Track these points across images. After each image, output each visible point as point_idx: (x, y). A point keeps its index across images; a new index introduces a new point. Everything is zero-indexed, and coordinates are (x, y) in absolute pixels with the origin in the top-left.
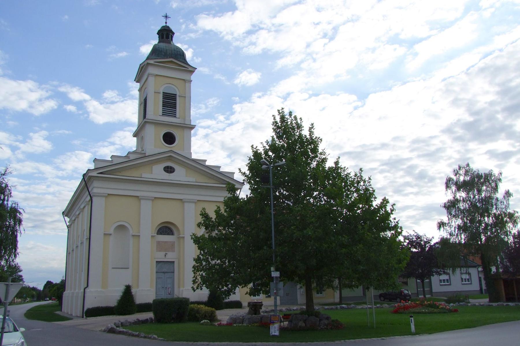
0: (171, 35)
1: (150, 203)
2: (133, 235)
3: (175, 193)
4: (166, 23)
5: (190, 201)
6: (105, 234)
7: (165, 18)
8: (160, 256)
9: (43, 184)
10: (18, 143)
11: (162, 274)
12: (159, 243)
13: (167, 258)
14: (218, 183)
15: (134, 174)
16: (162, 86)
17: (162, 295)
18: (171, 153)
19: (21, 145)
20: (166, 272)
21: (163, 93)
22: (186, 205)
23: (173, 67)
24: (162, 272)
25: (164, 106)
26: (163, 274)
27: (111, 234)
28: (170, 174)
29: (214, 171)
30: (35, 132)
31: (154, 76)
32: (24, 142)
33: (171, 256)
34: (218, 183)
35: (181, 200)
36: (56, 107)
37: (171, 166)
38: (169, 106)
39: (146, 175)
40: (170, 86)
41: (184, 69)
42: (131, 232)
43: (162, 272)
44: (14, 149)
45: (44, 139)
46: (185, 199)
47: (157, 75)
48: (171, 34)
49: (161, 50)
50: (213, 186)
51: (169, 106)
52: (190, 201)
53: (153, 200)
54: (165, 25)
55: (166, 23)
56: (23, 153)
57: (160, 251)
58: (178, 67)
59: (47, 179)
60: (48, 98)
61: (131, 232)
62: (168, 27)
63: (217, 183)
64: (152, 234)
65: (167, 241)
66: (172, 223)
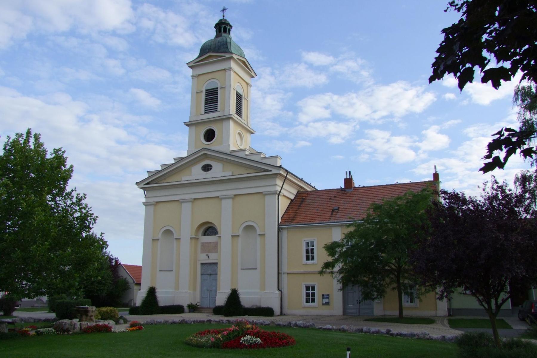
0: (229, 29)
1: (189, 205)
2: (259, 235)
3: (182, 194)
4: (224, 16)
5: (227, 198)
6: (153, 240)
7: (225, 11)
8: (203, 258)
9: (456, 179)
10: (417, 143)
11: (207, 275)
12: (203, 244)
13: (210, 259)
14: (257, 171)
15: (175, 179)
16: (204, 84)
17: (207, 297)
18: (204, 150)
19: (420, 145)
20: (211, 274)
21: (206, 90)
22: (223, 201)
23: (212, 61)
24: (208, 274)
25: (206, 103)
26: (208, 276)
27: (158, 240)
28: (208, 172)
29: (247, 160)
30: (426, 129)
31: (196, 77)
32: (421, 141)
33: (213, 258)
34: (257, 171)
35: (218, 197)
36: (435, 99)
37: (208, 163)
38: (211, 102)
39: (185, 178)
40: (216, 81)
41: (224, 58)
42: (258, 232)
43: (208, 274)
44: (416, 149)
45: (438, 133)
46: (264, 192)
47: (199, 75)
48: (229, 27)
49: (206, 48)
50: (253, 176)
51: (211, 102)
52: (227, 198)
53: (233, 198)
54: (222, 18)
55: (224, 16)
56: (424, 152)
57: (203, 253)
58: (215, 60)
59: (456, 174)
60: (424, 93)
61: (258, 232)
62: (226, 20)
63: (256, 172)
64: (191, 235)
65: (211, 242)
66: (211, 223)
